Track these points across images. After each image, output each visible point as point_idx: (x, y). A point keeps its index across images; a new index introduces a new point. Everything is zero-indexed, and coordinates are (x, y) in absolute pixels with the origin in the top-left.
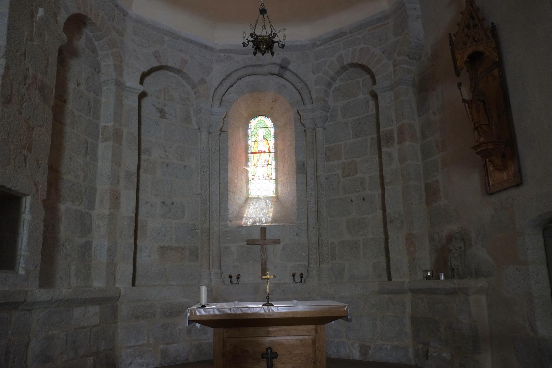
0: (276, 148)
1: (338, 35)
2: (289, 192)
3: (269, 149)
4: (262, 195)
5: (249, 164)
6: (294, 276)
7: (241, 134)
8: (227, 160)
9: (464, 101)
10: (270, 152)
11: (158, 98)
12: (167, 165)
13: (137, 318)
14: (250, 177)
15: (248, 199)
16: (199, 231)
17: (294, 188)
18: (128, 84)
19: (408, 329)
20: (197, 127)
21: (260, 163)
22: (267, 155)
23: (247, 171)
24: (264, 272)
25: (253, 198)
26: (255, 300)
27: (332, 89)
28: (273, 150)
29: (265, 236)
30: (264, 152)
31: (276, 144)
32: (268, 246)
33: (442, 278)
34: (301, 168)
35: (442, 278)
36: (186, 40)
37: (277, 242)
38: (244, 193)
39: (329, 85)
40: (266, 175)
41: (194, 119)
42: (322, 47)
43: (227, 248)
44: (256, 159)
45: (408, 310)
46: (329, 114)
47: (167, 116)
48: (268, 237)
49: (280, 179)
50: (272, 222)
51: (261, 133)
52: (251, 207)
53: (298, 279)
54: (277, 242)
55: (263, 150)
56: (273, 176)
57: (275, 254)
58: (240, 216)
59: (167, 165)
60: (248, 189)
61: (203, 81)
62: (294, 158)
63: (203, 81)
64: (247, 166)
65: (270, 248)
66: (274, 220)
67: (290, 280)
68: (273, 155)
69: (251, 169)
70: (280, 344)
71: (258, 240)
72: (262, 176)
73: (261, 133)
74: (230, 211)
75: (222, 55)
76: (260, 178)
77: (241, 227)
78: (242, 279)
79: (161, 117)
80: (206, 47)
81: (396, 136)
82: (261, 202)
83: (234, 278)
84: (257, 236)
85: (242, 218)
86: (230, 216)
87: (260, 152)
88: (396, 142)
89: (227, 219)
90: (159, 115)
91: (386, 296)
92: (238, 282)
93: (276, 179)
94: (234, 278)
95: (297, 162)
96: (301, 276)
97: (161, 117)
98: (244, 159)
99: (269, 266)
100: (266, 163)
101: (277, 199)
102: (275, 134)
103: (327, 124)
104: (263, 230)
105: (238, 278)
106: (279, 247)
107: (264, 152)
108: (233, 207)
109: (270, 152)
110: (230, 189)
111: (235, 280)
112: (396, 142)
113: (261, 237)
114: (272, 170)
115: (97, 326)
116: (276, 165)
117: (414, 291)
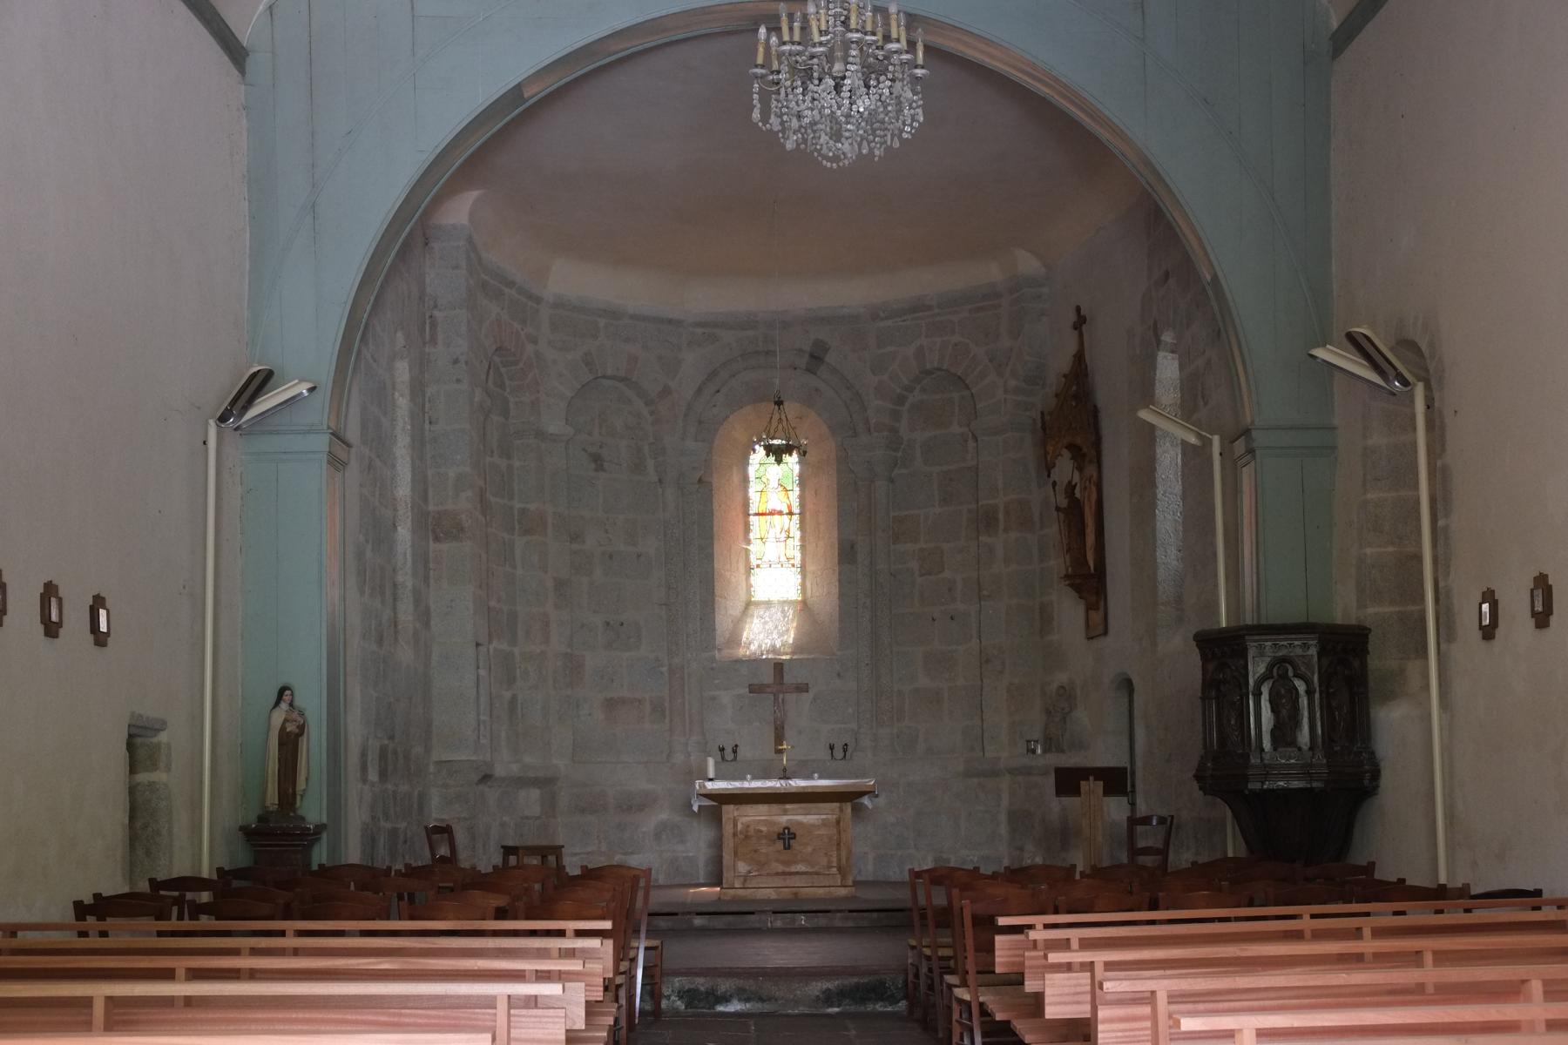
0: (802, 505)
1: (918, 307)
2: (826, 598)
3: (789, 507)
4: (775, 598)
5: (752, 536)
6: (832, 748)
7: (736, 479)
8: (712, 538)
9: (1058, 509)
10: (791, 513)
11: (590, 434)
12: (611, 557)
13: (583, 811)
14: (754, 562)
15: (749, 604)
16: (664, 669)
17: (835, 590)
18: (552, 429)
19: (1003, 829)
20: (655, 479)
21: (771, 535)
22: (786, 518)
23: (747, 551)
24: (779, 739)
25: (758, 604)
26: (603, 918)
27: (907, 405)
28: (796, 510)
29: (782, 677)
30: (780, 513)
31: (802, 497)
32: (788, 696)
33: (1039, 751)
34: (847, 554)
35: (1039, 751)
36: (634, 317)
37: (802, 688)
38: (742, 596)
39: (901, 400)
40: (783, 559)
41: (650, 463)
42: (889, 323)
43: (713, 698)
44: (764, 528)
45: (1005, 802)
46: (900, 454)
47: (606, 465)
48: (787, 679)
49: (810, 568)
50: (793, 653)
51: (772, 485)
52: (756, 621)
53: (839, 753)
54: (802, 688)
55: (778, 508)
56: (798, 561)
57: (799, 711)
58: (734, 639)
59: (611, 557)
60: (749, 586)
61: (666, 392)
62: (835, 534)
63: (666, 392)
64: (749, 542)
65: (791, 698)
66: (798, 648)
67: (826, 755)
68: (796, 518)
69: (755, 548)
70: (800, 824)
71: (768, 686)
72: (774, 558)
73: (772, 485)
74: (718, 632)
75: (699, 331)
76: (774, 567)
77: (739, 661)
78: (741, 753)
79: (596, 470)
80: (670, 321)
81: (1001, 516)
82: (773, 610)
83: (728, 751)
84: (767, 677)
85: (739, 644)
86: (719, 640)
87: (772, 513)
88: (1001, 526)
89: (714, 647)
90: (593, 466)
91: (975, 780)
92: (735, 759)
93: (803, 567)
94: (728, 751)
95: (841, 542)
96: (845, 748)
97: (596, 470)
98: (741, 527)
99: (788, 733)
100: (784, 535)
101: (805, 607)
102: (801, 476)
103: (896, 471)
104: (779, 667)
105: (735, 752)
106: (806, 698)
107: (780, 513)
108: (723, 623)
109: (791, 513)
110: (718, 591)
111: (729, 755)
112: (1001, 526)
113: (773, 680)
114: (794, 550)
115: (538, 818)
116: (803, 539)
117: (1013, 771)
